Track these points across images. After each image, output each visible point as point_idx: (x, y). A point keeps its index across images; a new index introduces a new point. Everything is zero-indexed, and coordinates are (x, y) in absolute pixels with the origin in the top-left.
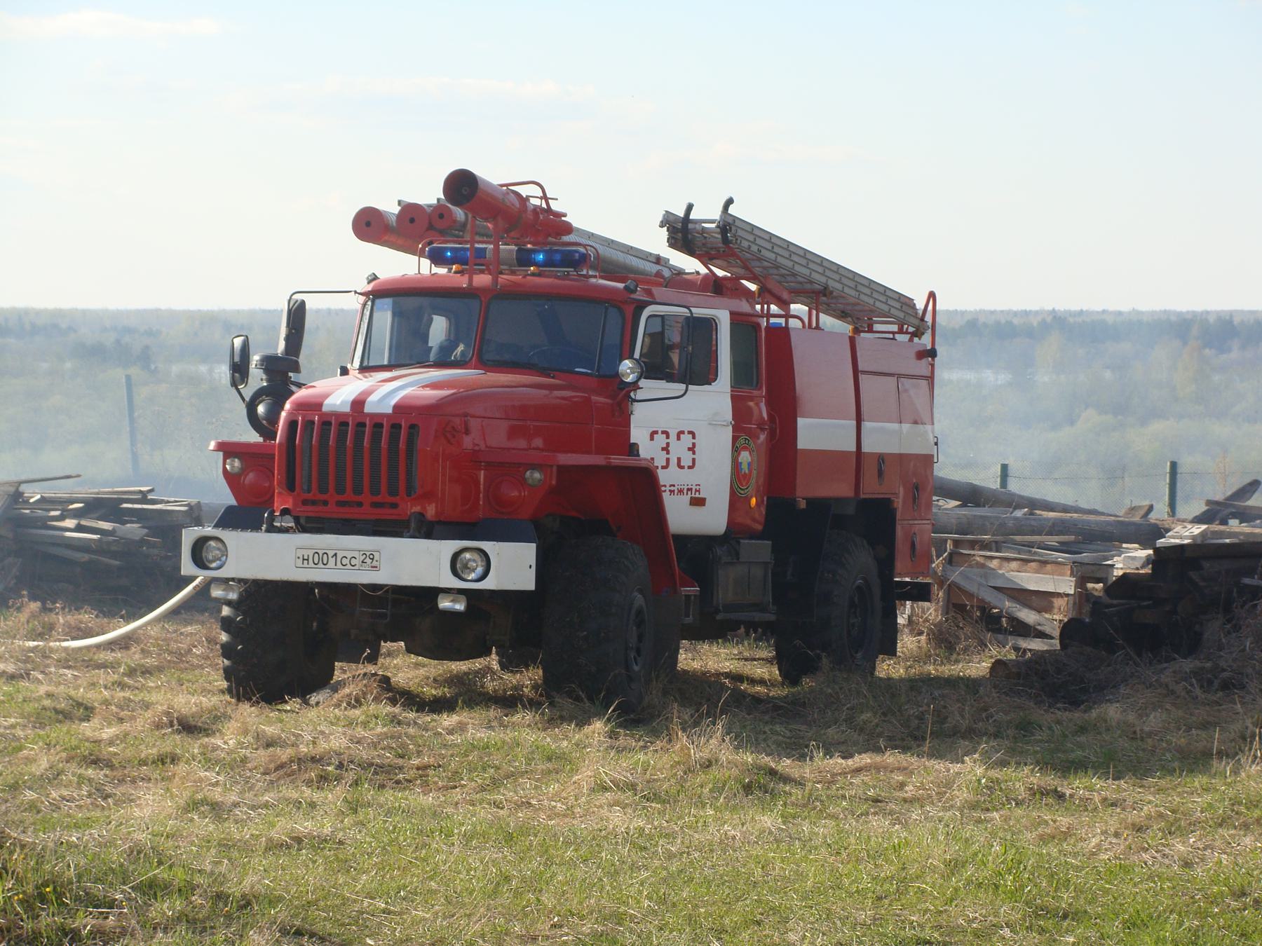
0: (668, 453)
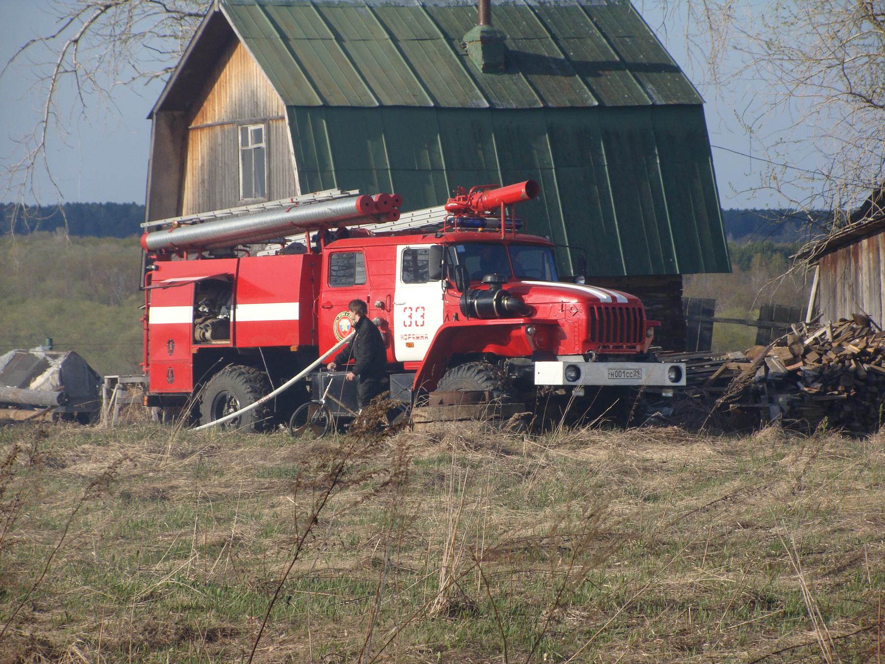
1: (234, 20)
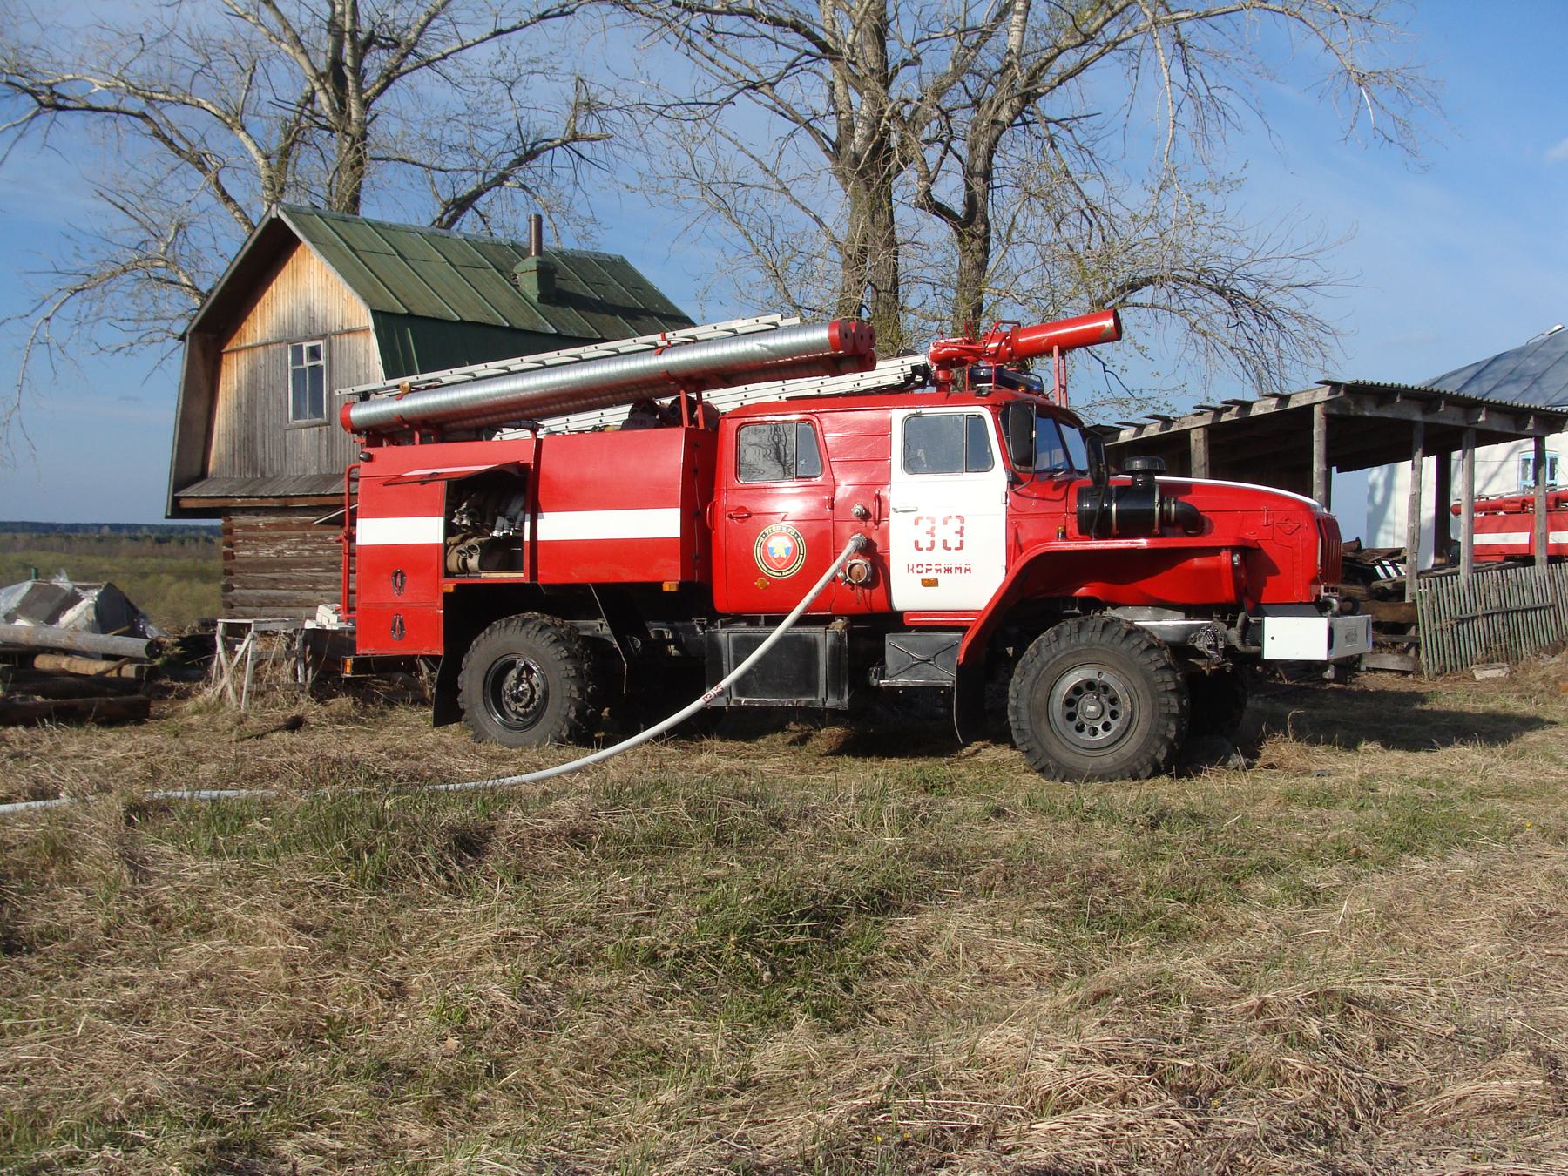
1: (297, 225)
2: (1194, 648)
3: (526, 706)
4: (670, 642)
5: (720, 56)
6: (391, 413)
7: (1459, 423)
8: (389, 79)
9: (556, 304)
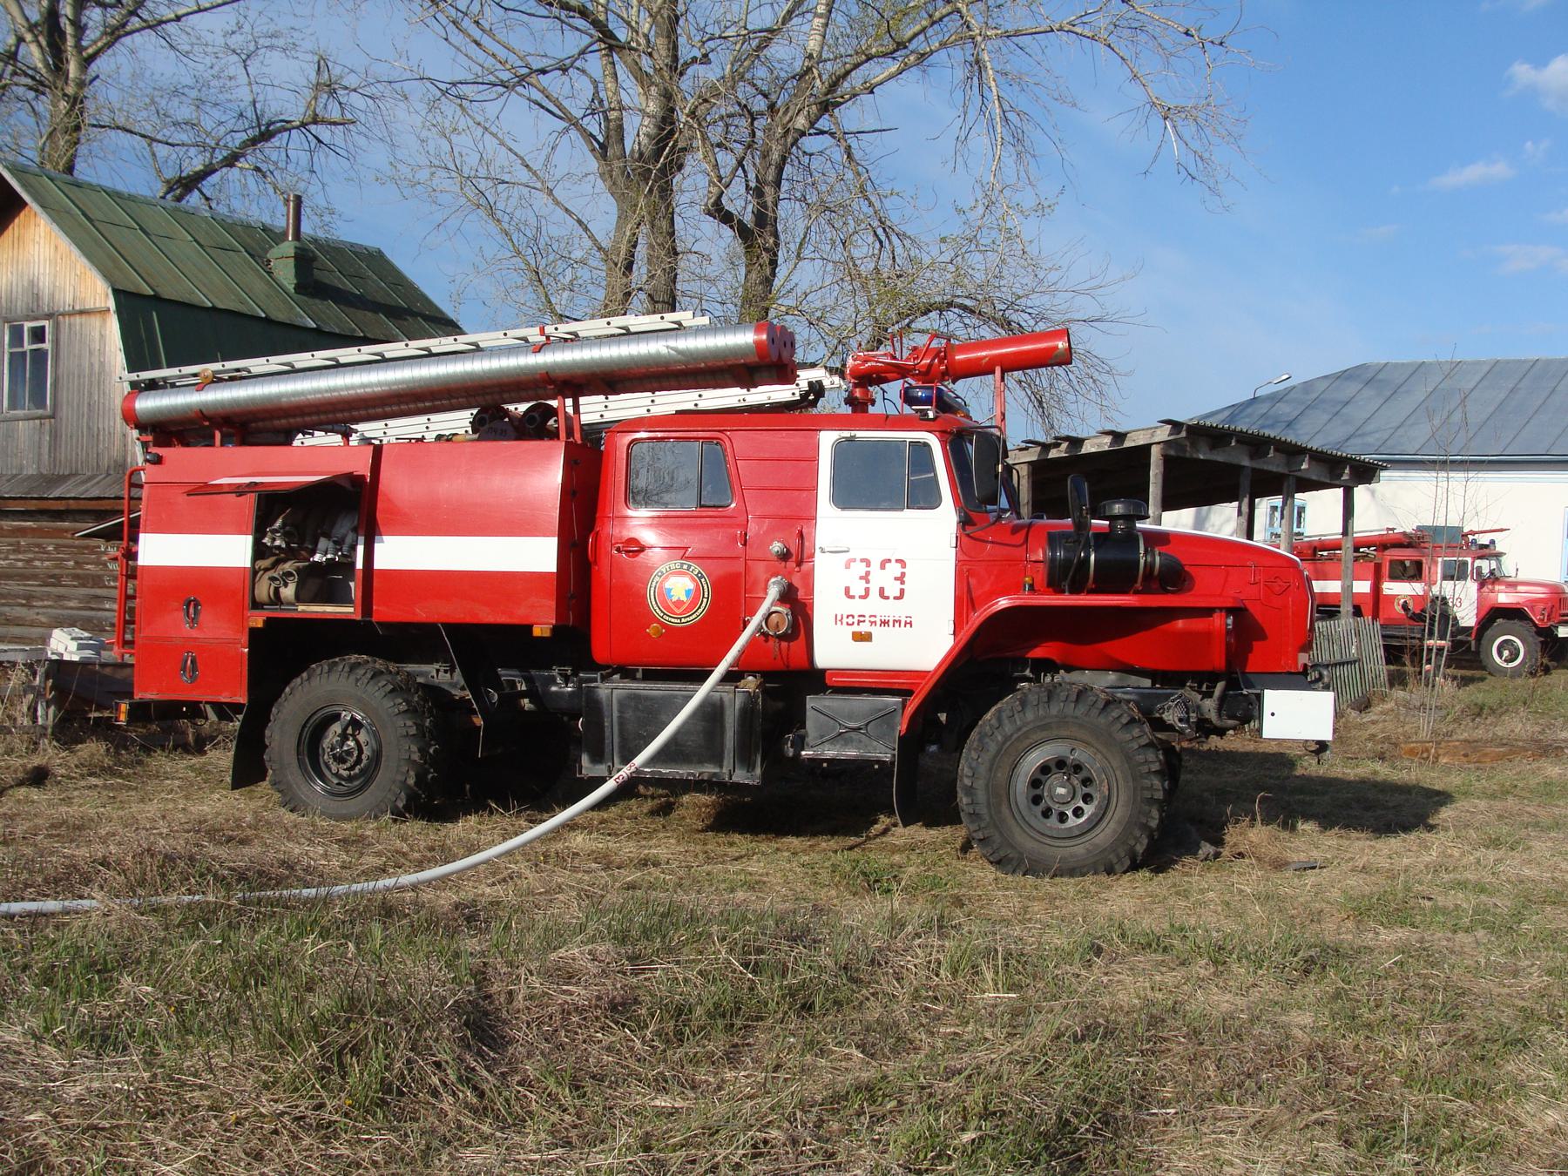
0: (868, 582)
2: (1161, 719)
3: (351, 768)
4: (523, 695)
5: (486, 41)
6: (189, 406)
7: (1281, 470)
8: (115, 34)
9: (312, 296)
